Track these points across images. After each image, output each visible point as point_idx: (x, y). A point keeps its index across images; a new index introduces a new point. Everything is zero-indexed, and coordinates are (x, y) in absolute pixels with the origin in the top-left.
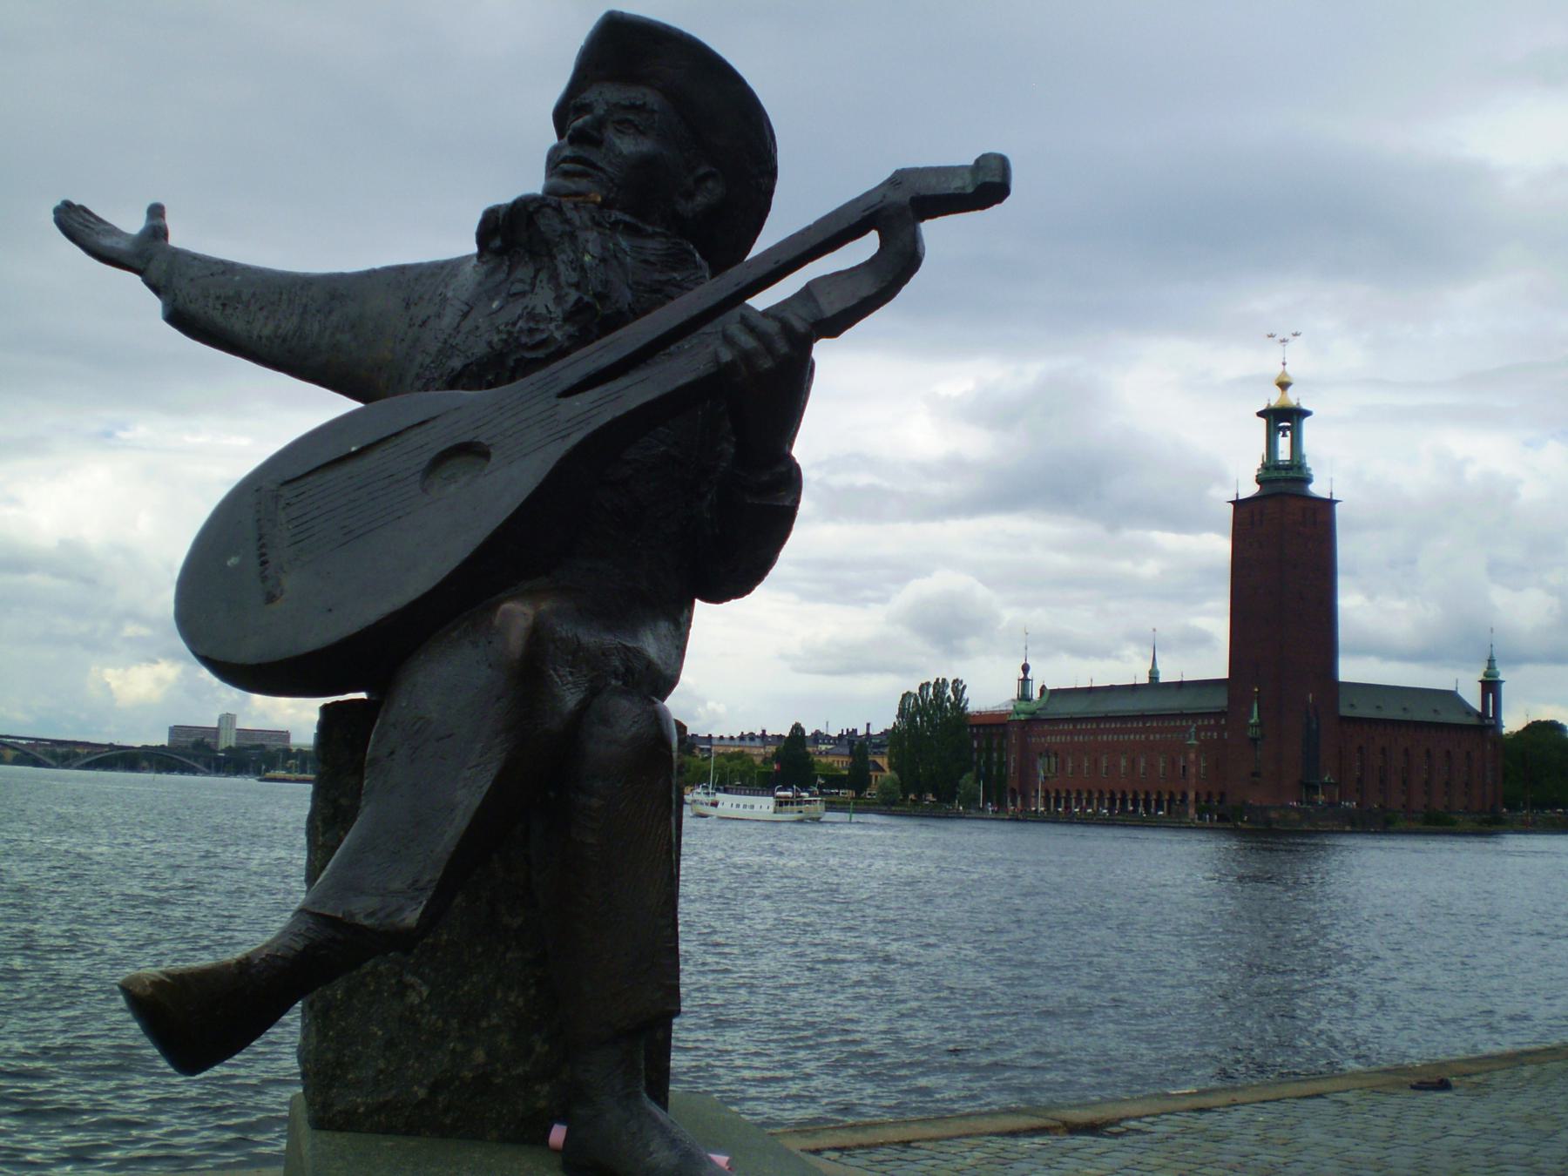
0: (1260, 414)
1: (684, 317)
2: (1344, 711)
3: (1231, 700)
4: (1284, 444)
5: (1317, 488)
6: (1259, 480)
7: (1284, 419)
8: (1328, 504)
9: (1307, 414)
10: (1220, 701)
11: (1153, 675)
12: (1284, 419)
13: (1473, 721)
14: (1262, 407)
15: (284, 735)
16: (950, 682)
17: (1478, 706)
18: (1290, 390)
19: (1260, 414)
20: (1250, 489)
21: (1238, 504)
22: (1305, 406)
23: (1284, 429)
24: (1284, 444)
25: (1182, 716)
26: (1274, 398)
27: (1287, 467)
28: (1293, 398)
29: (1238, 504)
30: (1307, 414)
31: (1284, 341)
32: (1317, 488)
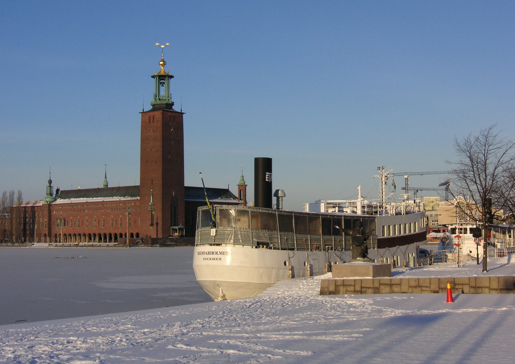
21: (143, 113)
26: (162, 70)
29: (143, 113)
32: (176, 108)
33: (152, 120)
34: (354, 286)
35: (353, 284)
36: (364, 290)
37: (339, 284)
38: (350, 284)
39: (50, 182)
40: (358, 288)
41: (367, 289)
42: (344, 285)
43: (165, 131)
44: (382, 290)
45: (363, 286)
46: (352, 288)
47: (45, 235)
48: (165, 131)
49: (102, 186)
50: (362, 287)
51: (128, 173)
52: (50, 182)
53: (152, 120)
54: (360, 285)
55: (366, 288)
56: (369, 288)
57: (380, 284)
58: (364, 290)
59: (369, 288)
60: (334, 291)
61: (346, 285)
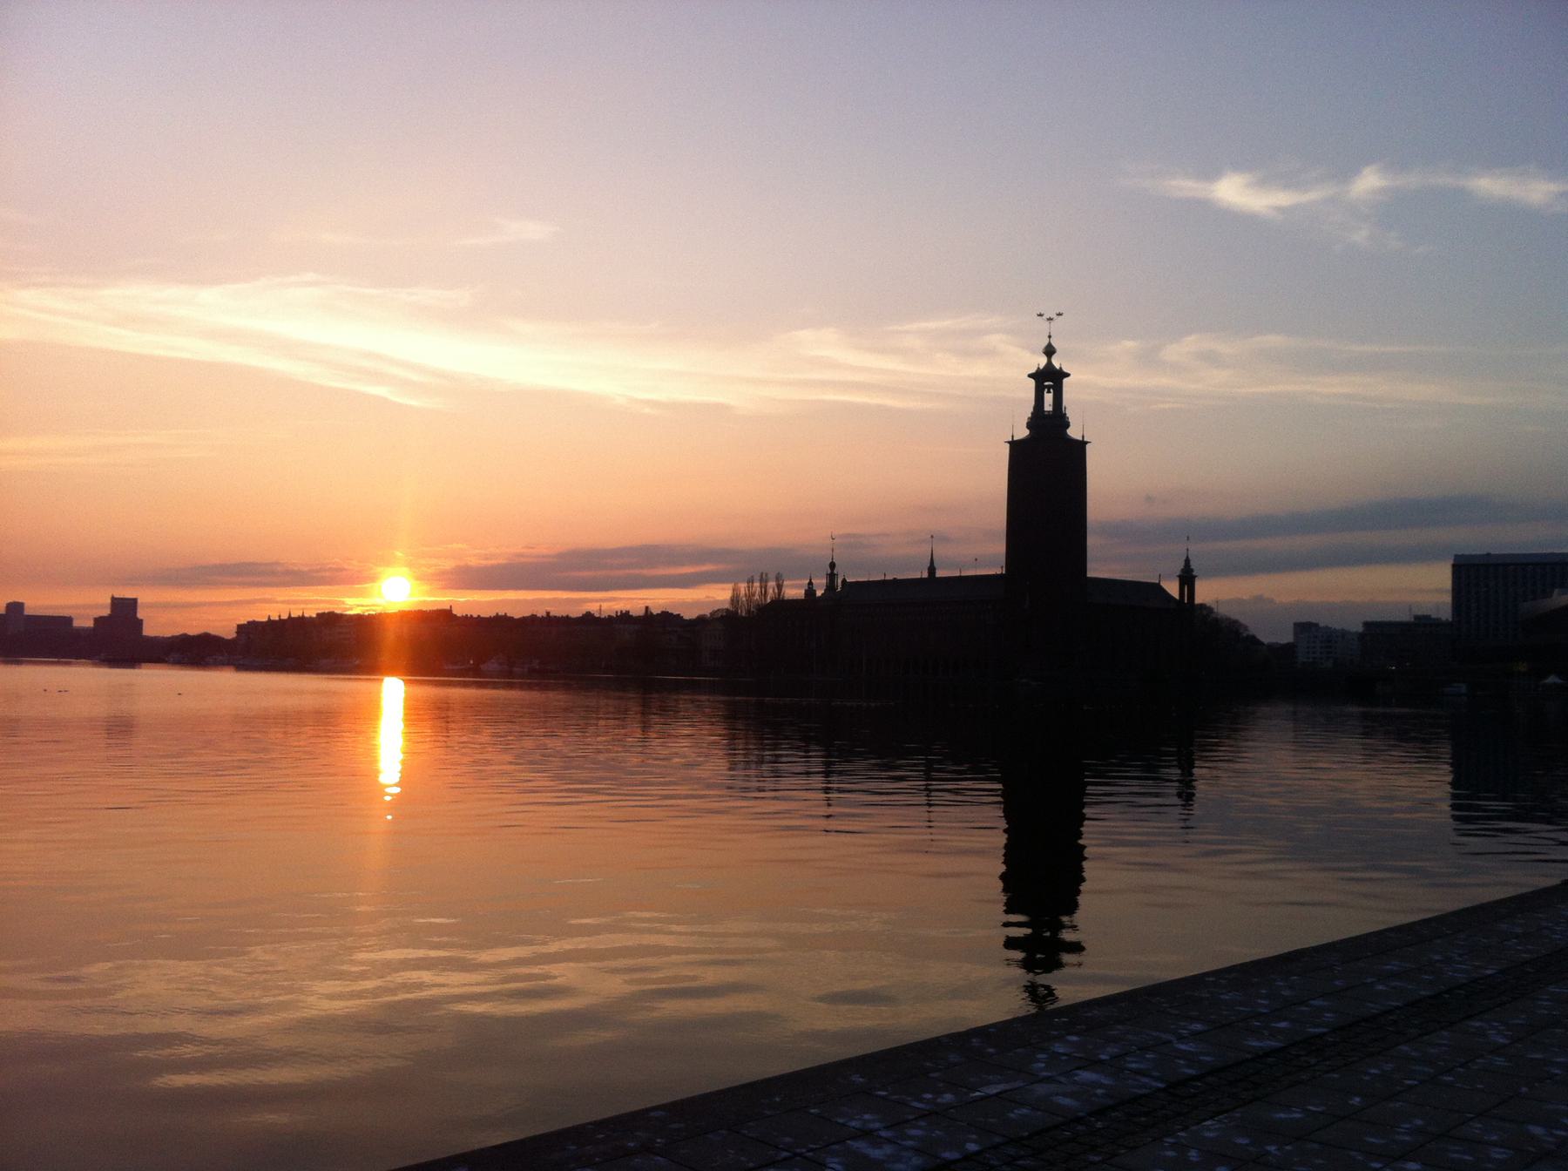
0: (1030, 376)
1: (262, 590)
4: (1049, 398)
5: (1074, 432)
6: (1029, 426)
7: (1050, 351)
8: (1082, 445)
9: (1068, 375)
12: (1050, 351)
15: (68, 620)
16: (772, 576)
17: (1176, 595)
19: (1030, 376)
20: (1022, 433)
21: (1015, 445)
23: (1049, 387)
24: (1049, 398)
27: (1050, 416)
30: (1068, 375)
31: (1050, 319)
32: (1074, 432)
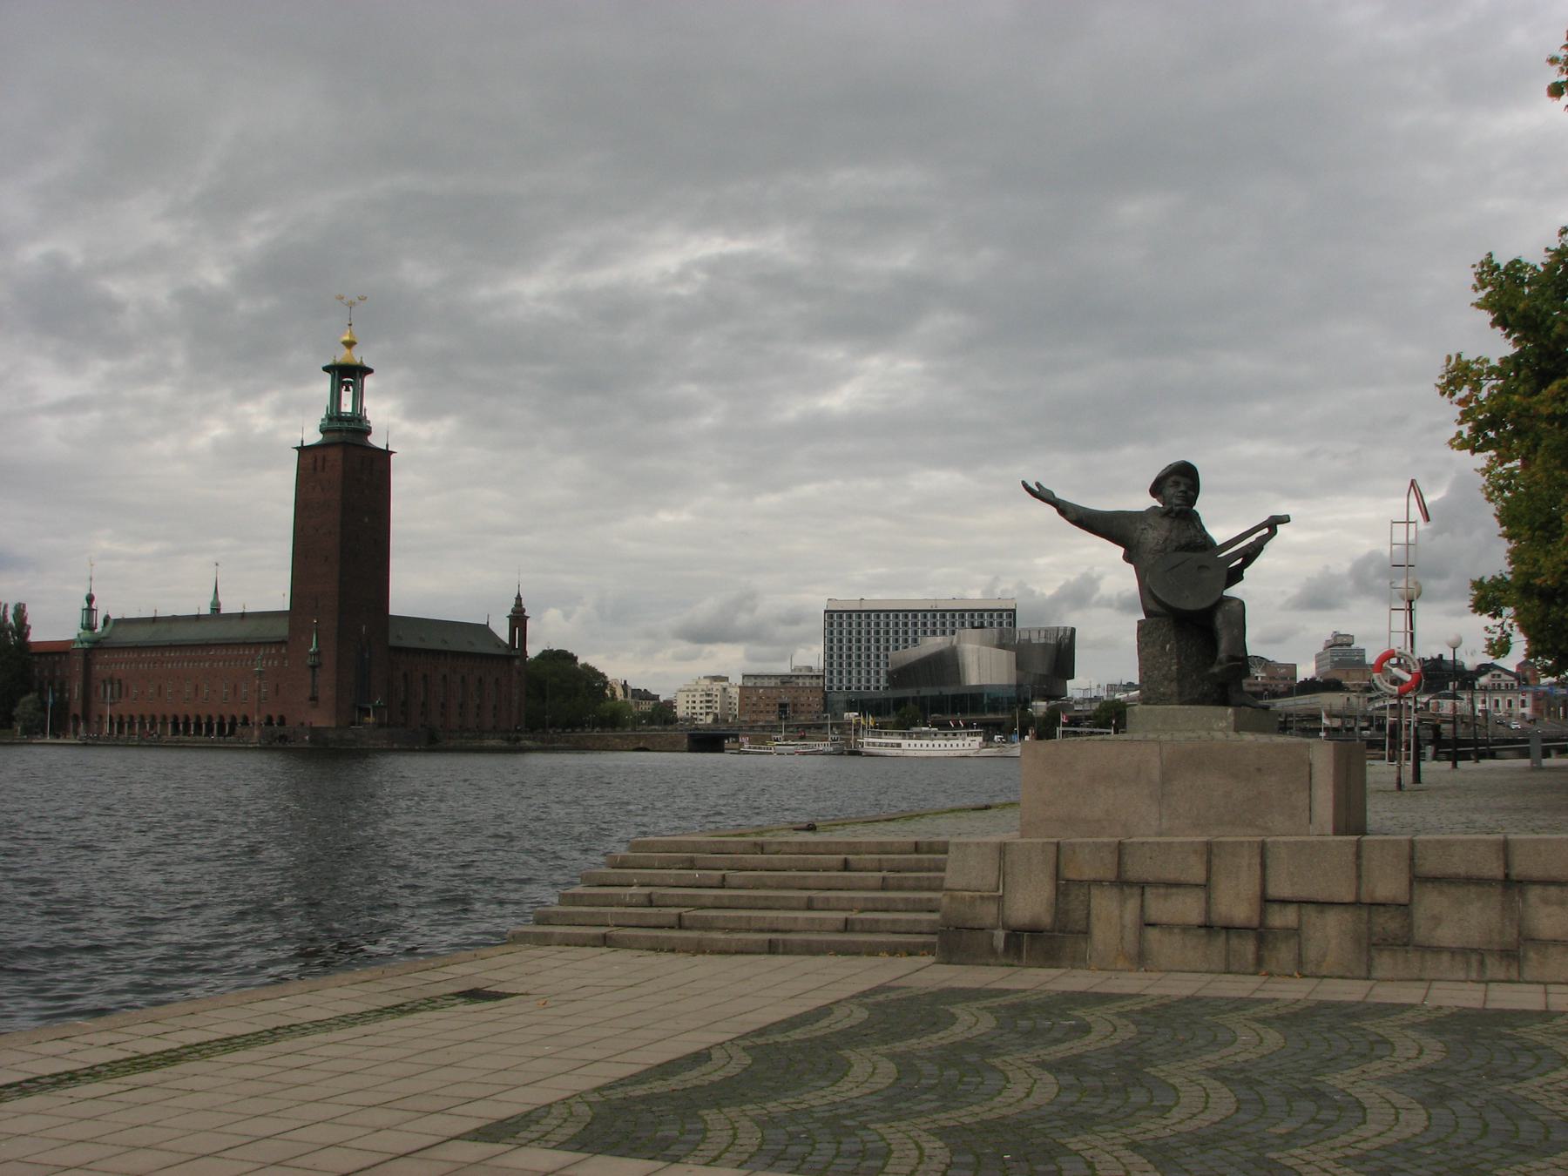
2: (393, 641)
3: (291, 628)
8: (387, 454)
10: (282, 630)
11: (216, 608)
13: (503, 652)
14: (328, 363)
18: (355, 348)
21: (302, 450)
22: (367, 364)
25: (245, 644)
26: (342, 356)
28: (358, 356)
30: (370, 371)
32: (376, 441)
33: (320, 463)
34: (1206, 886)
35: (1197, 873)
36: (1282, 918)
37: (1088, 873)
38: (1171, 874)
39: (90, 599)
40: (1236, 904)
41: (1311, 913)
42: (1121, 882)
43: (345, 489)
44: (1437, 920)
45: (1274, 891)
46: (1188, 908)
47: (76, 717)
48: (345, 489)
49: (206, 610)
50: (1266, 901)
51: (263, 582)
52: (90, 599)
53: (320, 463)
54: (1247, 885)
55: (1301, 903)
56: (1323, 905)
57: (1418, 879)
58: (1282, 918)
59: (1323, 905)
60: (1046, 920)
61: (1143, 885)
